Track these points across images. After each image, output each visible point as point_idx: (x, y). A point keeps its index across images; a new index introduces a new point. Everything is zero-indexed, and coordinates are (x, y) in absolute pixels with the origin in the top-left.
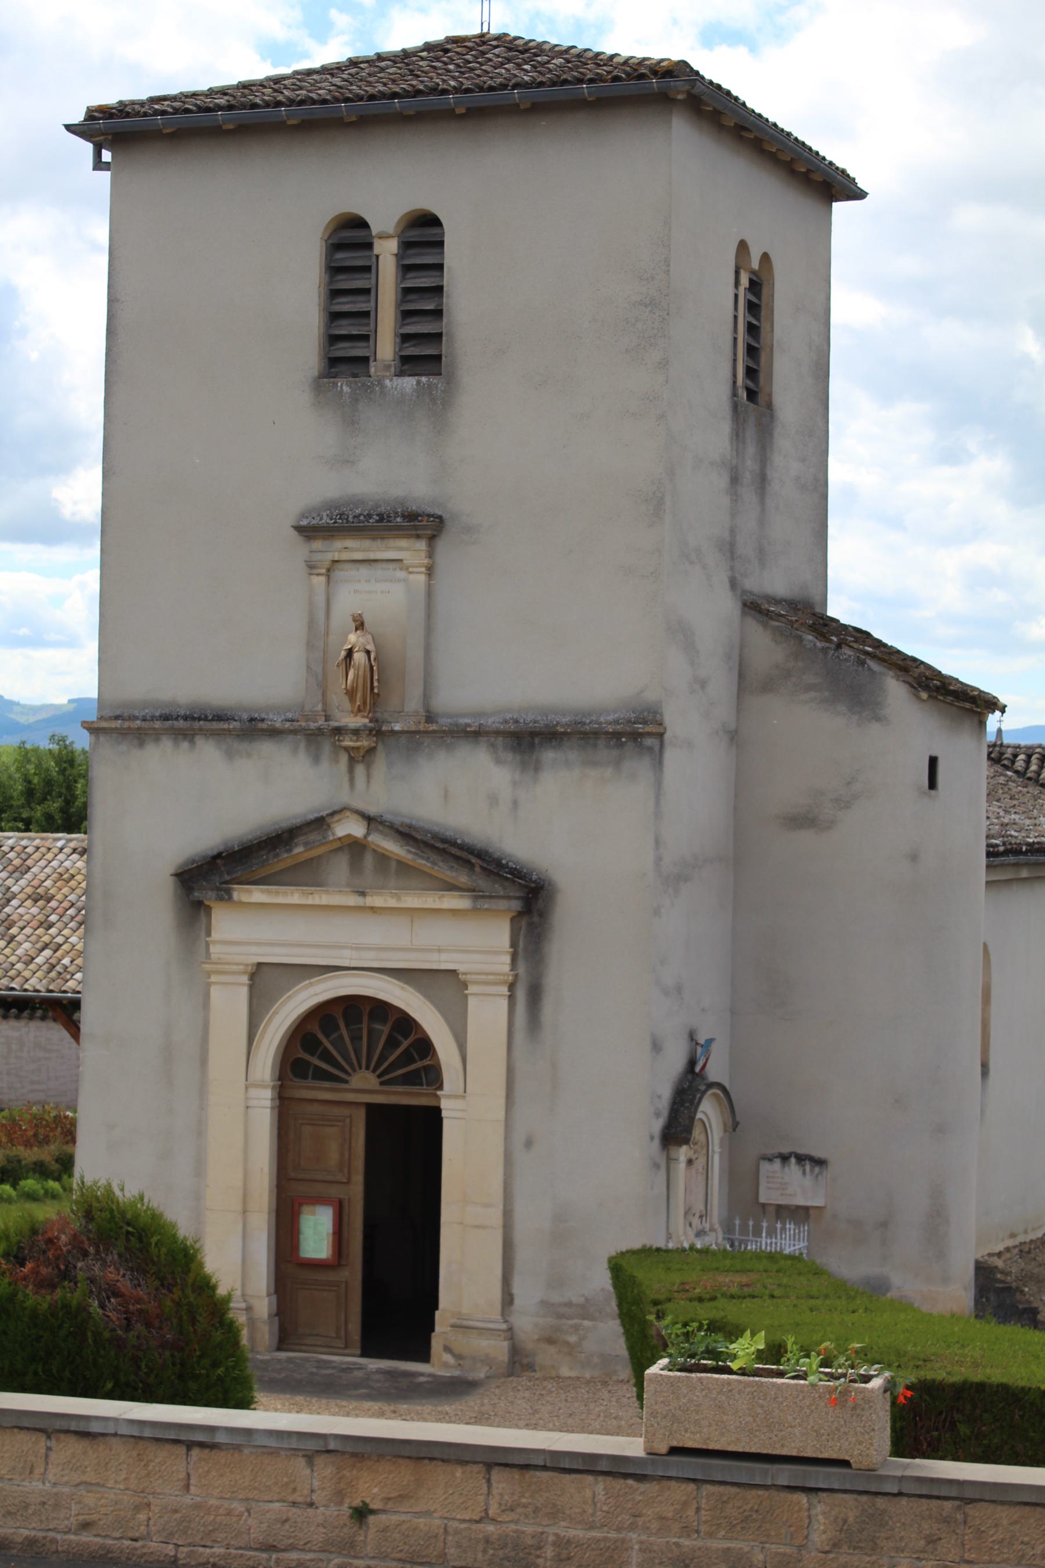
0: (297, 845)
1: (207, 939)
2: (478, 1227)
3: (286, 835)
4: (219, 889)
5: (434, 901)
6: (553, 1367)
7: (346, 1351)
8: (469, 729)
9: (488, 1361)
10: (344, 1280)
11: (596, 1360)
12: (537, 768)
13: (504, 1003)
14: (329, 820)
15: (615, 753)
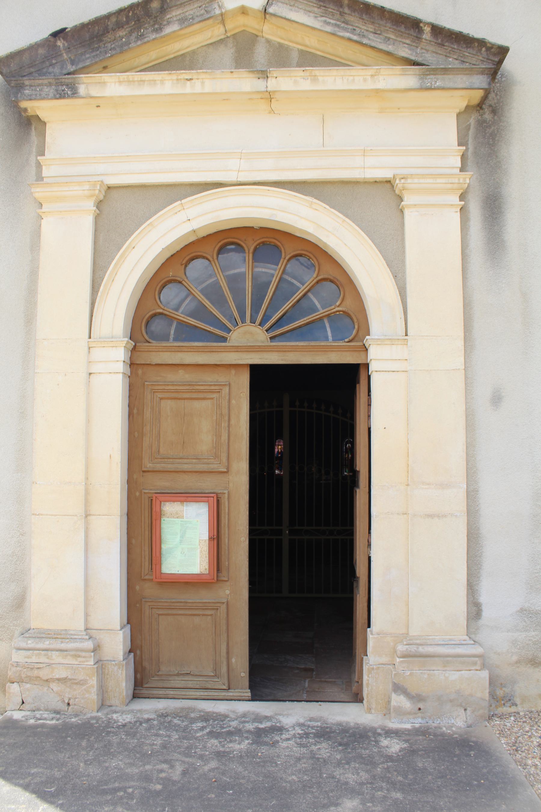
0: (169, 23)
1: (39, 158)
2: (431, 516)
5: (365, 80)
7: (230, 694)
10: (225, 601)
13: (457, 217)
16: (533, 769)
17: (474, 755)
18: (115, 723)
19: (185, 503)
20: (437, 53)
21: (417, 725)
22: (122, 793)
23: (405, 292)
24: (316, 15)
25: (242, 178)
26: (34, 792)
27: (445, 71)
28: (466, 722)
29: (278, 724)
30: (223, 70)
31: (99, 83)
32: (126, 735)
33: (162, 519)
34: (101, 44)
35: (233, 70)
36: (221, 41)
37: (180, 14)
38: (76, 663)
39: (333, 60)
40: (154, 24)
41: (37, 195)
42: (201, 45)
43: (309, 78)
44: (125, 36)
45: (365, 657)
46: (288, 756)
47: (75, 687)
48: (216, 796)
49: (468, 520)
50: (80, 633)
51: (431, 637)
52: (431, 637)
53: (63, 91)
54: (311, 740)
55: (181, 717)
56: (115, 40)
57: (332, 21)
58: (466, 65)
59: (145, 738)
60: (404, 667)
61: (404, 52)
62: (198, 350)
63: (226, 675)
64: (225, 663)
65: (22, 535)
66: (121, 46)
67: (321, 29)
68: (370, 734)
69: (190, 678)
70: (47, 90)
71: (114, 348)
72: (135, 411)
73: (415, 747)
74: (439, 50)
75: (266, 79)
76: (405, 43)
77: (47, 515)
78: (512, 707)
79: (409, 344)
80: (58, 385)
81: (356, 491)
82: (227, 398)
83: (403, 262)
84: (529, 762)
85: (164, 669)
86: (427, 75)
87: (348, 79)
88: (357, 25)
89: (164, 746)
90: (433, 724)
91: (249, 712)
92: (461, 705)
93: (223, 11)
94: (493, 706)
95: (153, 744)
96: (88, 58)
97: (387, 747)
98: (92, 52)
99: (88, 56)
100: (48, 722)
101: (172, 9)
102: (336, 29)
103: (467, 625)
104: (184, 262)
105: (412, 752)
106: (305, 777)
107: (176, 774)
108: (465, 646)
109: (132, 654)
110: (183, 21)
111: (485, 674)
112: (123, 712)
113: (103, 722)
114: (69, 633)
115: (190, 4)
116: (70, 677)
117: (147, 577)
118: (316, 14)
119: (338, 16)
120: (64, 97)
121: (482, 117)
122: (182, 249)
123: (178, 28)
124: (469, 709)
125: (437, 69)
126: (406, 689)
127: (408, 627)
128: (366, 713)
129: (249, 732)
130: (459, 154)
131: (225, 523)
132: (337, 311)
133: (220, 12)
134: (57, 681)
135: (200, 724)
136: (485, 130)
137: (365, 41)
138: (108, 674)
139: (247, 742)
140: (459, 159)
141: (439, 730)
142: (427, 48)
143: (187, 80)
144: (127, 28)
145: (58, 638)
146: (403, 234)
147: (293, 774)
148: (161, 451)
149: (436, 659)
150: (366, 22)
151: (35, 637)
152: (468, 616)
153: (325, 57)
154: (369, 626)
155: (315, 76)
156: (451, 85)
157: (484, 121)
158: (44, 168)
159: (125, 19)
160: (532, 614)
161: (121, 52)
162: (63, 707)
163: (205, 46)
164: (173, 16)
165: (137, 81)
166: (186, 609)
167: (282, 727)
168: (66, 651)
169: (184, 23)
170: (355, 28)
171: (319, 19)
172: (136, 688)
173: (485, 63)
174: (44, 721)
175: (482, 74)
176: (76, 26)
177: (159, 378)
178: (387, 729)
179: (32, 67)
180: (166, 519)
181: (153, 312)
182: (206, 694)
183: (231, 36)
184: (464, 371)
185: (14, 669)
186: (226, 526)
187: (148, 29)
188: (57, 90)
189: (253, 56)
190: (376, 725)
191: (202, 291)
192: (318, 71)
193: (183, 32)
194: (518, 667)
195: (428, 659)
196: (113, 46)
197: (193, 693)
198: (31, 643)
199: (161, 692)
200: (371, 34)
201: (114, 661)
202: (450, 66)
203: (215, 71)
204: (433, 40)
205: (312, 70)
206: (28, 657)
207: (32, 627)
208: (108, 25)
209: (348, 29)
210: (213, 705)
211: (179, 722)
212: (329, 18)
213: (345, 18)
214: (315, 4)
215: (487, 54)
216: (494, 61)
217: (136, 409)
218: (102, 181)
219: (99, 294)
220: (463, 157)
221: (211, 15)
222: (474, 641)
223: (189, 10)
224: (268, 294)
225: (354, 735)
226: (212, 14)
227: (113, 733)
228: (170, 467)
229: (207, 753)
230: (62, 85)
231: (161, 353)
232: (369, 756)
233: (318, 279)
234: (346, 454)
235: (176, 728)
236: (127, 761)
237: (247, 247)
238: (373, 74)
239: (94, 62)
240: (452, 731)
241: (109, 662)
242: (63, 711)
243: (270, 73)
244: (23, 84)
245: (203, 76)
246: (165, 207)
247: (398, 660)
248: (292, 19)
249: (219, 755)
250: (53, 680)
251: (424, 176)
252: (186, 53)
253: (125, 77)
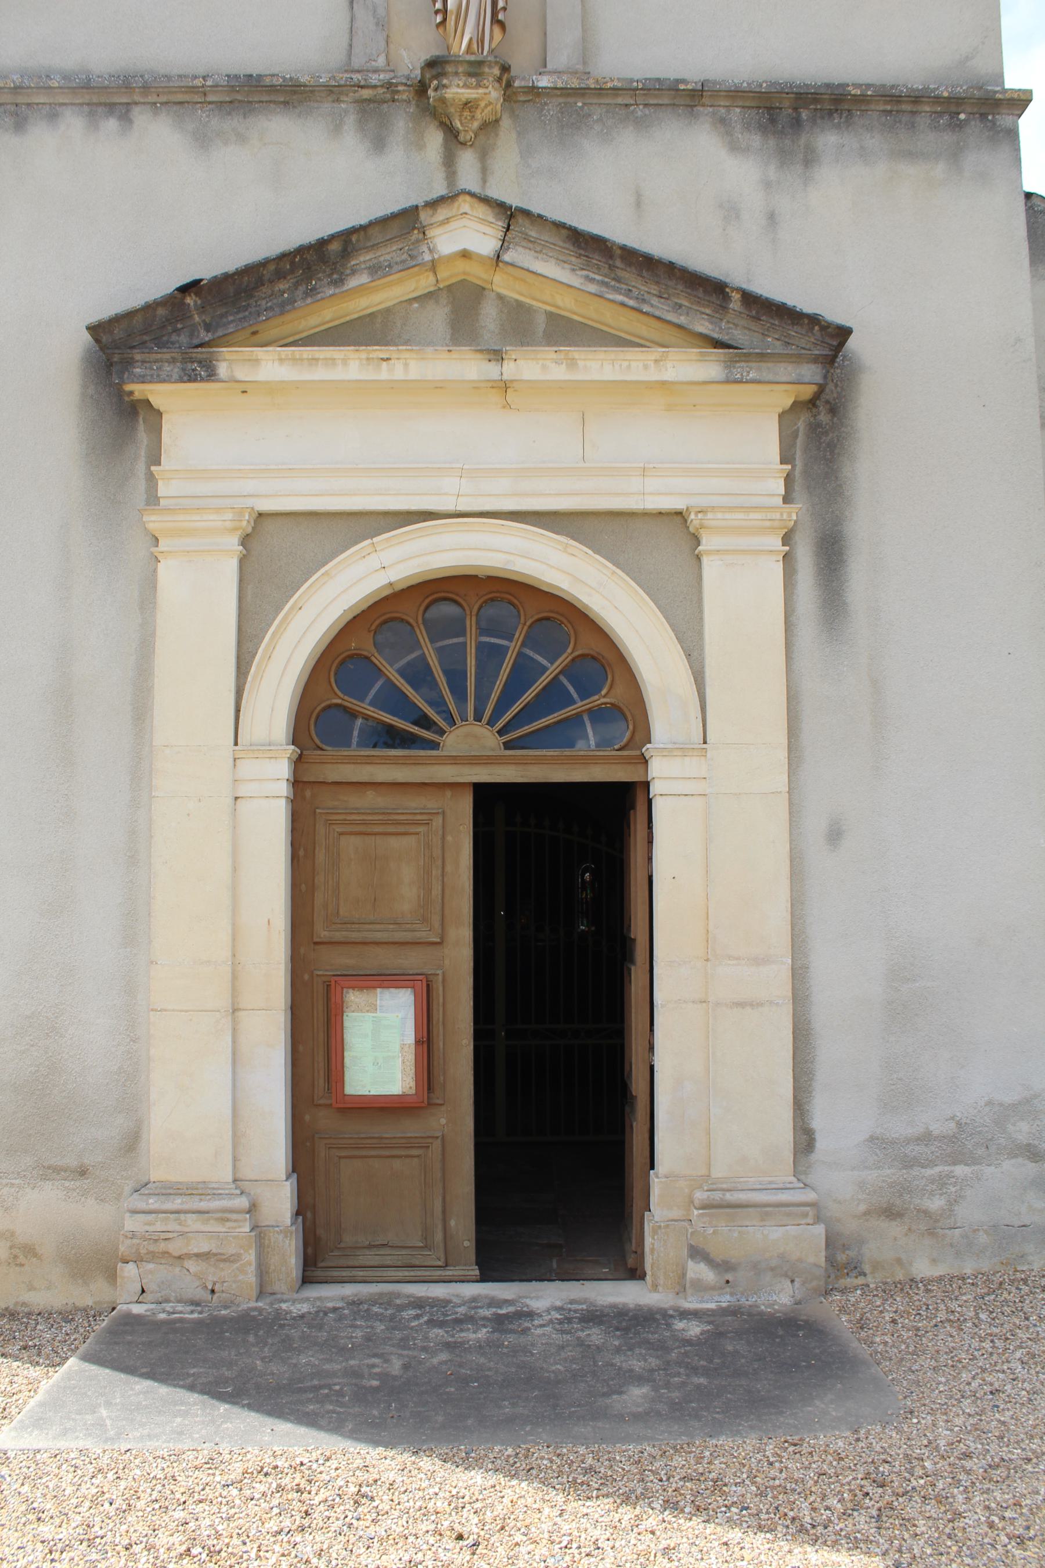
0: (354, 272)
1: (153, 468)
2: (741, 1005)
3: (335, 247)
4: (188, 359)
5: (646, 367)
6: (899, 1261)
7: (448, 1273)
8: (682, 87)
9: (787, 1269)
11: (983, 1238)
12: (810, 160)
13: (779, 568)
14: (424, 216)
15: (948, 137)
16: (881, 1347)
17: (803, 1335)
18: (287, 1314)
19: (379, 990)
20: (750, 330)
21: (724, 1305)
22: (326, 1391)
23: (703, 678)
25: (462, 508)
26: (203, 1392)
27: (762, 357)
28: (793, 1297)
29: (525, 1309)
31: (249, 360)
32: (309, 1328)
33: (345, 1014)
34: (252, 302)
35: (451, 348)
36: (429, 295)
37: (370, 260)
38: (224, 1230)
39: (598, 329)
40: (332, 274)
41: (151, 526)
44: (288, 289)
45: (647, 1213)
46: (547, 1344)
47: (222, 1265)
48: (457, 1390)
49: (794, 1010)
50: (226, 1187)
51: (742, 1180)
52: (742, 1180)
53: (193, 370)
54: (575, 1326)
55: (381, 1304)
56: (272, 295)
58: (791, 349)
59: (338, 1331)
60: (704, 1223)
61: (703, 327)
62: (395, 761)
63: (441, 1245)
64: (440, 1227)
65: (134, 1041)
66: (282, 305)
67: (581, 287)
68: (658, 1316)
69: (388, 1251)
70: (168, 369)
71: (273, 760)
72: (301, 853)
73: (721, 1329)
74: (753, 325)
76: (703, 313)
77: (173, 1010)
78: (859, 1278)
79: (708, 755)
80: (188, 815)
81: (630, 970)
82: (440, 832)
83: (700, 634)
84: (878, 1339)
85: (348, 1239)
86: (736, 362)
87: (621, 365)
88: (633, 284)
89: (368, 1338)
90: (747, 1301)
91: (479, 1295)
92: (786, 1275)
94: (833, 1276)
95: (352, 1337)
96: (232, 321)
97: (683, 1330)
98: (237, 313)
99: (231, 318)
100: (187, 1316)
102: (604, 289)
103: (794, 1161)
104: (373, 627)
105: (719, 1334)
106: (574, 1366)
107: (396, 1366)
108: (792, 1191)
109: (301, 1217)
110: (375, 270)
111: (820, 1230)
112: (294, 1301)
113: (269, 1313)
114: (210, 1186)
116: (214, 1251)
117: (322, 1102)
119: (606, 271)
120: (195, 380)
121: (815, 419)
122: (370, 607)
124: (797, 1279)
125: (750, 354)
126: (708, 1254)
127: (709, 1166)
128: (650, 1292)
129: (484, 1318)
130: (781, 475)
131: (438, 1019)
132: (602, 704)
133: (430, 258)
134: (194, 1258)
135: (412, 1312)
136: (820, 438)
137: (646, 308)
138: (268, 1247)
139: (485, 1330)
140: (782, 482)
141: (756, 1309)
142: (736, 321)
143: (383, 359)
145: (192, 1194)
146: (700, 600)
147: (557, 1364)
148: (341, 912)
149: (750, 1210)
151: (158, 1194)
152: (795, 1148)
153: (585, 324)
154: (652, 1167)
156: (770, 377)
157: (819, 425)
158: (160, 483)
159: (288, 267)
160: (886, 1143)
161: (282, 313)
162: (204, 1295)
163: (406, 301)
166: (382, 1147)
167: (532, 1311)
168: (208, 1212)
172: (306, 1269)
173: (818, 347)
174: (182, 1315)
175: (815, 363)
176: (216, 277)
177: (336, 803)
178: (682, 1309)
179: (144, 334)
180: (350, 1014)
181: (328, 703)
182: (412, 1274)
183: (444, 287)
184: (787, 795)
185: (128, 1242)
186: (441, 1023)
188: (184, 370)
190: (666, 1306)
191: (402, 672)
192: (577, 353)
193: (373, 284)
194: (867, 1220)
195: (739, 1210)
196: (269, 304)
197: (393, 1273)
198: (153, 1203)
199: (345, 1273)
200: (654, 298)
201: (278, 1226)
202: (769, 351)
204: (742, 310)
206: (149, 1224)
207: (152, 1180)
208: (263, 275)
209: (621, 289)
210: (425, 1289)
211: (381, 1311)
215: (822, 335)
216: (831, 345)
217: (302, 849)
218: (253, 508)
219: (249, 678)
220: (789, 480)
222: (805, 1185)
224: (500, 677)
225: (635, 1317)
226: (419, 260)
227: (289, 1325)
228: (354, 936)
229: (432, 1344)
230: (193, 362)
231: (340, 766)
232: (659, 1341)
233: (573, 655)
234: (582, 892)
235: (380, 1318)
236: (322, 1357)
237: (469, 606)
238: (658, 358)
239: (240, 327)
240: (774, 1309)
241: (271, 1229)
242: (205, 1302)
243: (506, 353)
244: (132, 358)
245: (407, 355)
246: (347, 548)
247: (696, 1212)
249: (448, 1346)
250: (189, 1256)
251: (731, 509)
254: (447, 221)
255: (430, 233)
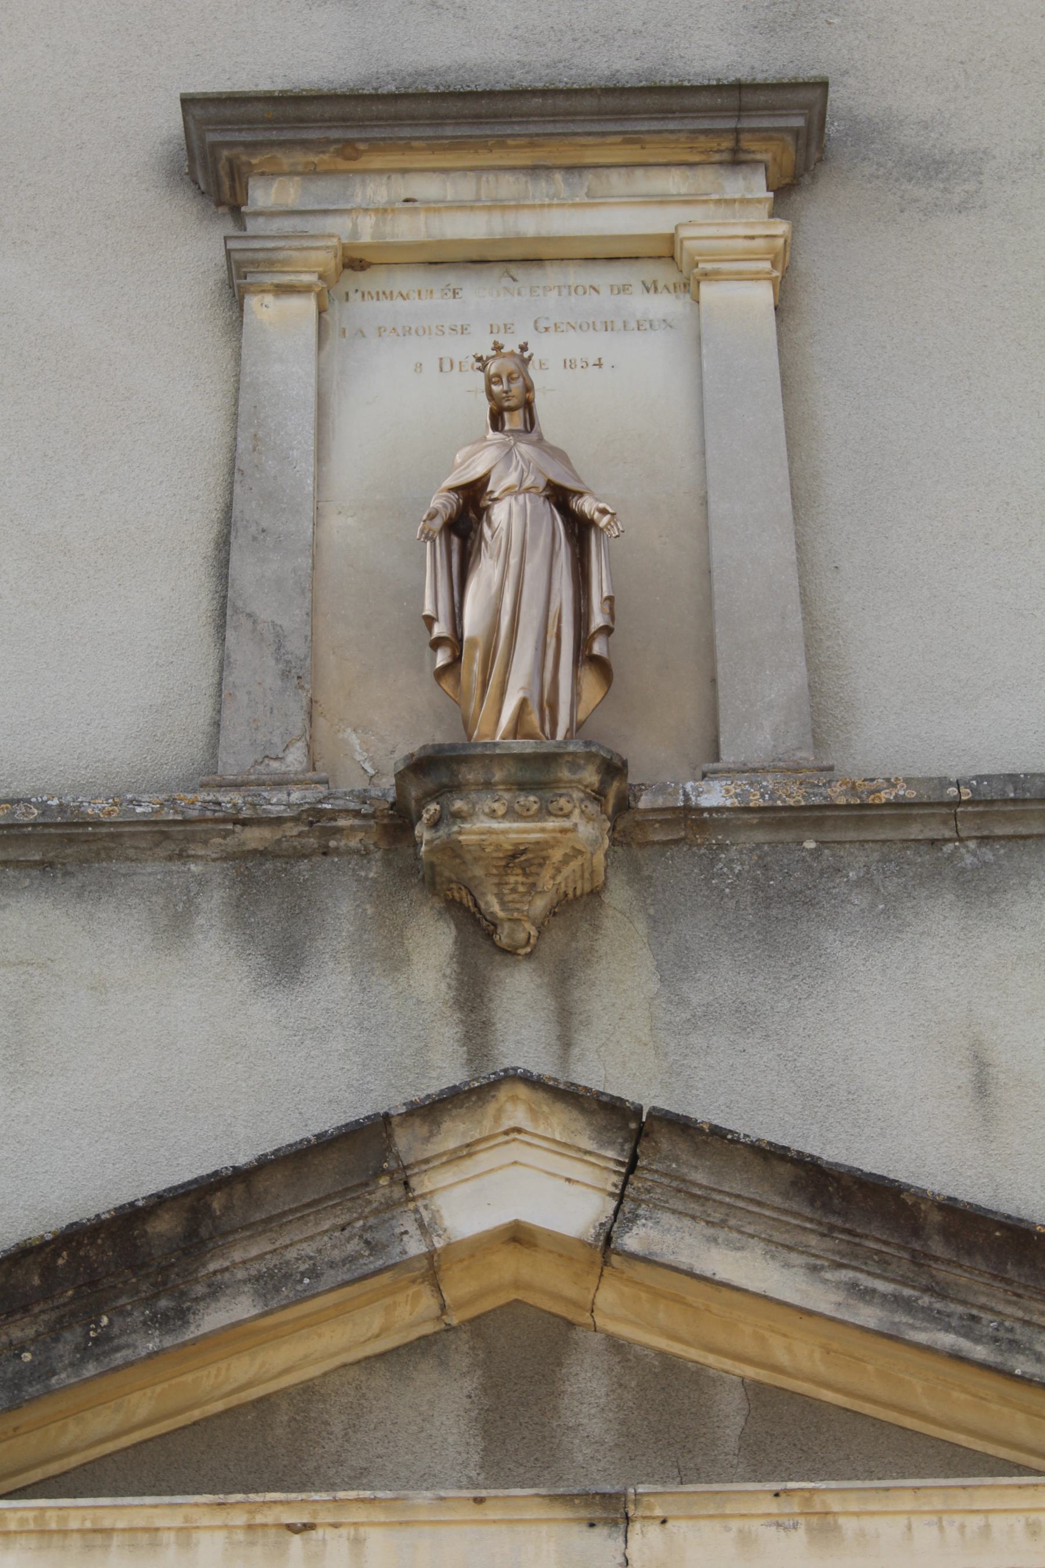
0: (215, 1291)
24: (812, 1261)
30: (443, 1493)
35: (483, 1493)
37: (261, 1257)
40: (156, 1296)
42: (337, 1361)
43: (802, 1520)
44: (34, 1340)
57: (882, 1286)
67: (838, 1315)
75: (622, 1526)
87: (962, 1528)
88: (982, 1300)
93: (439, 1243)
101: (231, 1239)
115: (302, 1217)
118: (814, 1255)
123: (254, 1312)
133: (424, 1249)
144: (43, 1312)
150: (1020, 1291)
155: (827, 1513)
159: (36, 1281)
163: (358, 1362)
164: (234, 1265)
165: (79, 1531)
169: (277, 1290)
170: (975, 1312)
171: (828, 1275)
183: (463, 1323)
187: (130, 1314)
189: (555, 1408)
203: (410, 1493)
205: (809, 1490)
212: (869, 1273)
213: (932, 1277)
214: (811, 1220)
221: (391, 1262)
223: (301, 1241)
243: (636, 1503)
245: (359, 1514)
248: (717, 1278)
252: (276, 1393)
253: (31, 1515)
254: (468, 1150)
255: (423, 1184)
